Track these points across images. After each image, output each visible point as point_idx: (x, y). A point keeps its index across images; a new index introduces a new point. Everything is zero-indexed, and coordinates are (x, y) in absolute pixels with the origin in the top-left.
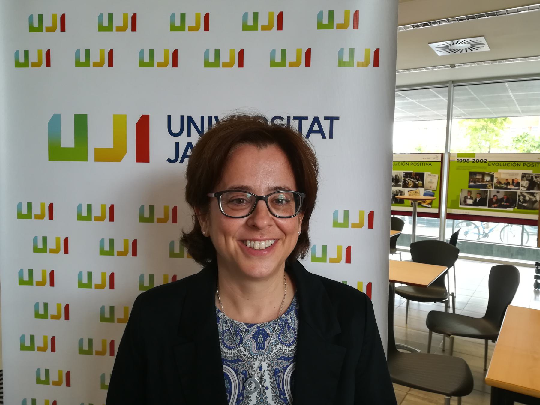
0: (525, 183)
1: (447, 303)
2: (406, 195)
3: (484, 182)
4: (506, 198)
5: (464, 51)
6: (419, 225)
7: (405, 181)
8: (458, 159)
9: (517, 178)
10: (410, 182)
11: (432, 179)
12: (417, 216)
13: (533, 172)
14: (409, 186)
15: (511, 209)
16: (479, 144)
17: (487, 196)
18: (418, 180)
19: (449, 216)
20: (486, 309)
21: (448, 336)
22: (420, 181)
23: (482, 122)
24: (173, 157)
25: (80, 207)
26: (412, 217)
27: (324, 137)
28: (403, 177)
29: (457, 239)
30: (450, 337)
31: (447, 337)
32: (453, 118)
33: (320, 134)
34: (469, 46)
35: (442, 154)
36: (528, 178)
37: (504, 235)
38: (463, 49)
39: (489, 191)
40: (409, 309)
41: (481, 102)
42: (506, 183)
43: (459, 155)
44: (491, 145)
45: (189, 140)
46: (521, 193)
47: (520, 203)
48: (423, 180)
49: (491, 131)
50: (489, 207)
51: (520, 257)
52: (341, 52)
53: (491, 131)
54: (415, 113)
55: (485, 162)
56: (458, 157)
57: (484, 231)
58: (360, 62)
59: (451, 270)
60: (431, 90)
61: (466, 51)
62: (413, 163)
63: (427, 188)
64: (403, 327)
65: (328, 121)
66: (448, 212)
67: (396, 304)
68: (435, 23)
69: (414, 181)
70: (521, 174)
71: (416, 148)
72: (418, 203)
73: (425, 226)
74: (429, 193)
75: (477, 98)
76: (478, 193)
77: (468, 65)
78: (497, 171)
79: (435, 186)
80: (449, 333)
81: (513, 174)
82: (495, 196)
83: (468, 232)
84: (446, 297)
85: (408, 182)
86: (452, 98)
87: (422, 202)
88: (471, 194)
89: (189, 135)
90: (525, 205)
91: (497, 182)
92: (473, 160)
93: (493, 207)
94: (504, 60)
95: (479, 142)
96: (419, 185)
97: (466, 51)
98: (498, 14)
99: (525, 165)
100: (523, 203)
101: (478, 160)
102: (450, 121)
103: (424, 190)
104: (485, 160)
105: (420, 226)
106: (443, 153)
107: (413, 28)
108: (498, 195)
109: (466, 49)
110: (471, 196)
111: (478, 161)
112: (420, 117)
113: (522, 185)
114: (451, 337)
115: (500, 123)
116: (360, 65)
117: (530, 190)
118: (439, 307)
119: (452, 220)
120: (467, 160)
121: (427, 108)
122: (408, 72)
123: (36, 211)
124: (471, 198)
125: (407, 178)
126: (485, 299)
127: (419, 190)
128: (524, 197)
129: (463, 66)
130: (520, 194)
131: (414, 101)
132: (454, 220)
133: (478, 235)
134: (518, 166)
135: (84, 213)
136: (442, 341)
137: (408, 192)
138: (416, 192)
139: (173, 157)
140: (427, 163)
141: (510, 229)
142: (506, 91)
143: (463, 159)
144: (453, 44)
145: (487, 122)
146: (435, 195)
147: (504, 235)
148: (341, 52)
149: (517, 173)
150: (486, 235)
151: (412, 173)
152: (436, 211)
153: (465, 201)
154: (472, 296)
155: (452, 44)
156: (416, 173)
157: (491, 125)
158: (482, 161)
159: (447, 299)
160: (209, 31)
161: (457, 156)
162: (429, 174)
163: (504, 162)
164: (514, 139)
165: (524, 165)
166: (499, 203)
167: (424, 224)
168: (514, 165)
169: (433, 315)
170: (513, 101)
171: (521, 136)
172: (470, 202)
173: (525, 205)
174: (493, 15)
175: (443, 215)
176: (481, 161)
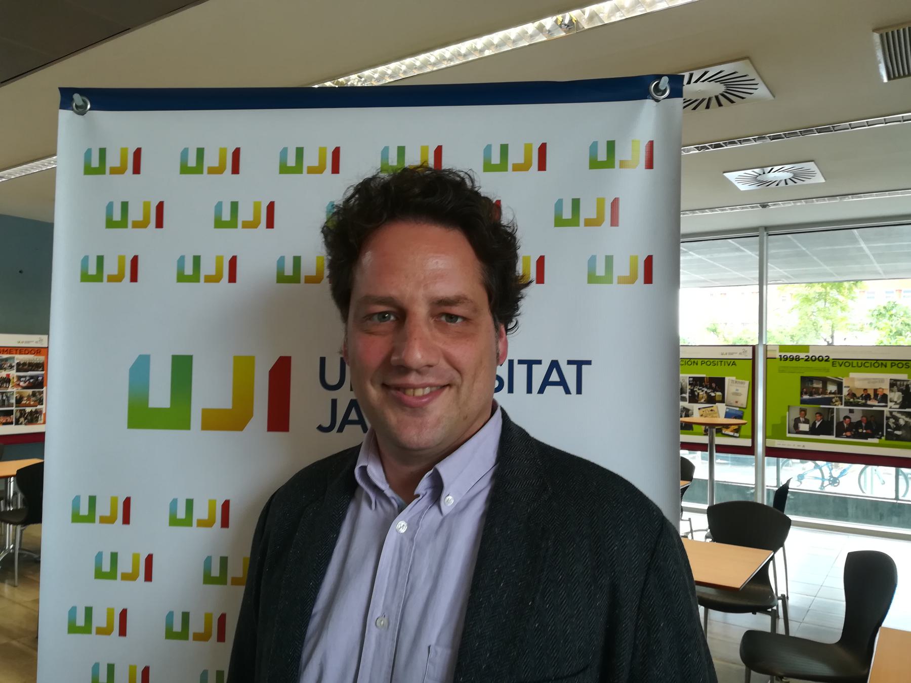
0: (896, 396)
1: (774, 616)
2: (696, 417)
3: (826, 394)
4: (865, 422)
5: (782, 184)
6: (719, 461)
8: (780, 356)
9: (883, 388)
10: (702, 393)
11: (738, 388)
12: (716, 452)
13: (909, 378)
14: (701, 400)
15: (876, 441)
16: (815, 324)
17: (833, 417)
18: (714, 390)
19: (771, 452)
21: (779, 679)
22: (717, 391)
23: (818, 288)
24: (327, 424)
25: (174, 504)
26: (708, 453)
27: (568, 391)
28: (690, 384)
29: (788, 488)
31: (777, 680)
32: (769, 283)
33: (561, 388)
34: (790, 175)
36: (901, 388)
37: (865, 482)
38: (781, 181)
41: (815, 258)
42: (864, 395)
43: (783, 348)
44: (835, 326)
46: (891, 413)
47: (889, 430)
49: (833, 303)
50: (837, 436)
51: (895, 519)
52: (592, 261)
53: (833, 303)
55: (826, 360)
56: (780, 351)
57: (831, 473)
59: (779, 554)
60: (730, 241)
61: (786, 184)
62: (705, 361)
63: (731, 404)
65: (574, 367)
66: (768, 445)
68: (734, 143)
70: (889, 381)
71: (708, 329)
72: (717, 429)
73: (729, 462)
75: (808, 252)
76: (817, 413)
77: (790, 203)
79: (743, 400)
80: (780, 673)
81: (875, 381)
82: (846, 417)
83: (803, 476)
84: (772, 604)
85: (698, 394)
86: (765, 253)
87: (723, 427)
88: (806, 414)
90: (898, 433)
92: (806, 356)
93: (845, 436)
94: (850, 196)
95: (814, 321)
96: (717, 399)
97: (786, 184)
98: (836, 128)
99: (895, 365)
100: (895, 429)
101: (813, 358)
102: (765, 287)
103: (726, 407)
104: (826, 357)
105: (721, 464)
107: (697, 151)
108: (851, 415)
109: (785, 180)
110: (806, 417)
111: (814, 359)
112: (713, 282)
113: (891, 399)
114: (783, 680)
115: (848, 289)
116: (623, 280)
117: (905, 409)
118: (760, 622)
119: (776, 458)
121: (724, 267)
122: (691, 215)
123: (102, 509)
124: (806, 422)
127: (717, 407)
128: (897, 419)
129: (781, 205)
130: (889, 415)
131: (703, 258)
132: (778, 458)
133: (820, 481)
134: (881, 367)
135: (181, 514)
137: (698, 410)
138: (712, 410)
139: (327, 424)
140: (729, 361)
141: (875, 470)
142: (856, 241)
143: (788, 354)
144: (764, 173)
145: (826, 288)
146: (745, 417)
147: (865, 482)
148: (592, 261)
149: (881, 380)
150: (834, 481)
151: (703, 378)
152: (747, 443)
153: (796, 427)
154: (815, 597)
155: (762, 173)
156: (710, 378)
157: (833, 293)
158: (821, 358)
159: (775, 608)
161: (778, 351)
162: (732, 381)
164: (873, 313)
165: (892, 366)
166: (855, 430)
167: (728, 460)
168: (876, 365)
169: (751, 638)
170: (867, 256)
171: (885, 308)
172: (804, 427)
173: (898, 433)
174: (827, 130)
175: (760, 449)
176: (820, 359)
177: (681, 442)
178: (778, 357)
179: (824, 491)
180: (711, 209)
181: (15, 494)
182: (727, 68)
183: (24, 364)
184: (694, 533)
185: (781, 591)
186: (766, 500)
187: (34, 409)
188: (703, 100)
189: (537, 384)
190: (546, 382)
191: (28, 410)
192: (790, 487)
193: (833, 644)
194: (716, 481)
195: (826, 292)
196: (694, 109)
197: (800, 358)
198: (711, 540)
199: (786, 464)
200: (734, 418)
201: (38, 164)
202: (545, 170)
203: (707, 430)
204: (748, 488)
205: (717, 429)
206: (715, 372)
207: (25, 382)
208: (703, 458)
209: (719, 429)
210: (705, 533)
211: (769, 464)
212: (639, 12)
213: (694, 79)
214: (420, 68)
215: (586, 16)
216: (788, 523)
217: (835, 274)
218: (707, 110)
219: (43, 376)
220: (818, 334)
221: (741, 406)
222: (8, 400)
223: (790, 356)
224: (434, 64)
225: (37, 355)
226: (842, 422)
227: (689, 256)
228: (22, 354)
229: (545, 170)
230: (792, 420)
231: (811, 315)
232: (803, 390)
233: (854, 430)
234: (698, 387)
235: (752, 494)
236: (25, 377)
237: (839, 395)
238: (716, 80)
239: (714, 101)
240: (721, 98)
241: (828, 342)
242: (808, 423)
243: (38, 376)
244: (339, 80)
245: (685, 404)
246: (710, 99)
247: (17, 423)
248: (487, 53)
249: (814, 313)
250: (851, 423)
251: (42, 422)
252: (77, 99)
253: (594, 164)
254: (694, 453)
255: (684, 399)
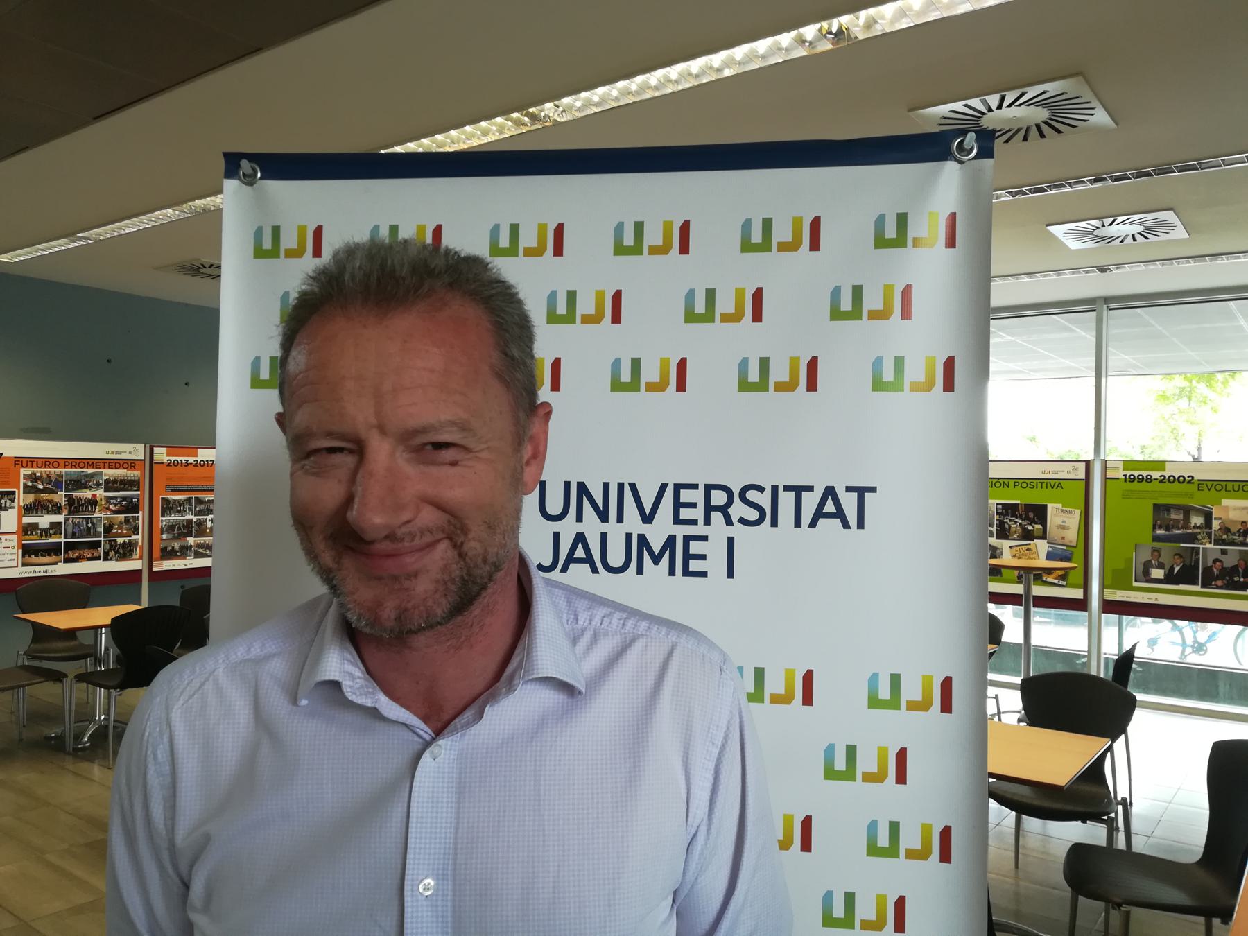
1: (1112, 828)
2: (1006, 559)
4: (1243, 567)
6: (1037, 619)
7: (1001, 524)
8: (1125, 475)
10: (1014, 525)
11: (1065, 519)
14: (1013, 535)
16: (1175, 431)
17: (1197, 561)
18: (1032, 522)
19: (1110, 607)
20: (1206, 834)
22: (1036, 523)
23: (1179, 381)
24: (548, 562)
26: (1022, 608)
27: (846, 525)
28: (997, 514)
29: (1133, 656)
30: (1119, 908)
31: (1114, 908)
32: (1109, 374)
34: (1140, 229)
35: (1088, 464)
38: (1127, 236)
39: (1203, 548)
40: (1021, 832)
42: (1241, 531)
43: (1128, 464)
45: (580, 528)
48: (1043, 520)
50: (1203, 586)
52: (878, 362)
54: (1020, 364)
55: (1189, 482)
57: (1195, 637)
58: (919, 382)
59: (1119, 744)
61: (1134, 240)
62: (1019, 482)
63: (1056, 540)
64: (1008, 877)
66: (1107, 597)
67: (992, 819)
69: (1024, 523)
72: (1035, 575)
73: (1053, 620)
74: (1060, 552)
76: (1176, 555)
78: (1220, 504)
79: (1072, 535)
80: (1117, 900)
82: (1215, 561)
83: (1156, 642)
85: (1010, 526)
88: (1160, 556)
89: (579, 518)
91: (1220, 529)
92: (1161, 476)
96: (1036, 534)
97: (1134, 240)
98: (1203, 166)
102: (1103, 380)
103: (1048, 545)
104: (1189, 477)
105: (1040, 622)
106: (1089, 461)
107: (1011, 198)
108: (1223, 558)
109: (1133, 235)
110: (1160, 560)
111: (1172, 480)
112: (1031, 373)
115: (1222, 383)
118: (1090, 833)
119: (1118, 616)
120: (1147, 476)
124: (1161, 566)
125: (1007, 517)
126: (1199, 810)
131: (1018, 341)
132: (1121, 616)
133: (1180, 649)
136: (1103, 914)
138: (1028, 549)
139: (548, 562)
140: (1053, 482)
143: (1136, 473)
144: (1103, 226)
145: (1191, 382)
146: (1075, 558)
148: (878, 362)
150: (1200, 648)
152: (1077, 594)
155: (1100, 227)
157: (1201, 388)
159: (1113, 815)
160: (632, 359)
163: (1234, 483)
167: (1050, 618)
169: (1079, 852)
172: (1158, 573)
175: (1095, 603)
176: (1181, 480)
177: (1046, 505)
178: (1121, 477)
179: (1184, 661)
180: (1028, 274)
181: (107, 649)
182: (1052, 88)
183: (115, 481)
184: (1002, 716)
185: (1122, 793)
186: (1102, 671)
187: (127, 539)
188: (1019, 130)
189: (807, 514)
190: (819, 514)
191: (120, 541)
192: (1136, 654)
193: (1193, 864)
194: (1033, 646)
195: (1190, 387)
196: (1007, 141)
197: (1153, 478)
198: (1026, 724)
199: (1130, 625)
200: (1058, 560)
201: (135, 222)
202: (818, 249)
203: (1022, 575)
204: (1078, 657)
205: (1035, 575)
206: (1033, 497)
207: (115, 505)
208: (1015, 615)
209: (1038, 575)
210: (1018, 715)
211: (1108, 624)
212: (932, 17)
213: (1006, 103)
214: (637, 93)
215: (861, 22)
216: (1131, 704)
217: (1203, 363)
218: (1025, 143)
219: (138, 497)
220: (1179, 445)
221: (1069, 544)
222: (94, 528)
223: (1139, 476)
224: (656, 88)
225: (131, 469)
226: (1212, 566)
227: (1002, 335)
228: (112, 468)
229: (818, 249)
230: (1141, 563)
231: (1169, 419)
232: (1156, 522)
233: (1227, 578)
234: (1009, 518)
235: (1084, 664)
236: (115, 498)
237: (1207, 530)
238: (1037, 104)
239: (1034, 131)
240: (1044, 127)
241: (1193, 456)
242: (1163, 568)
243: (131, 498)
244: (529, 110)
245: (993, 541)
246: (1028, 129)
247: (106, 558)
248: (727, 73)
249: (1174, 416)
250: (1223, 568)
251: (137, 557)
252: (245, 165)
253: (881, 242)
254: (1002, 608)
255: (991, 535)
